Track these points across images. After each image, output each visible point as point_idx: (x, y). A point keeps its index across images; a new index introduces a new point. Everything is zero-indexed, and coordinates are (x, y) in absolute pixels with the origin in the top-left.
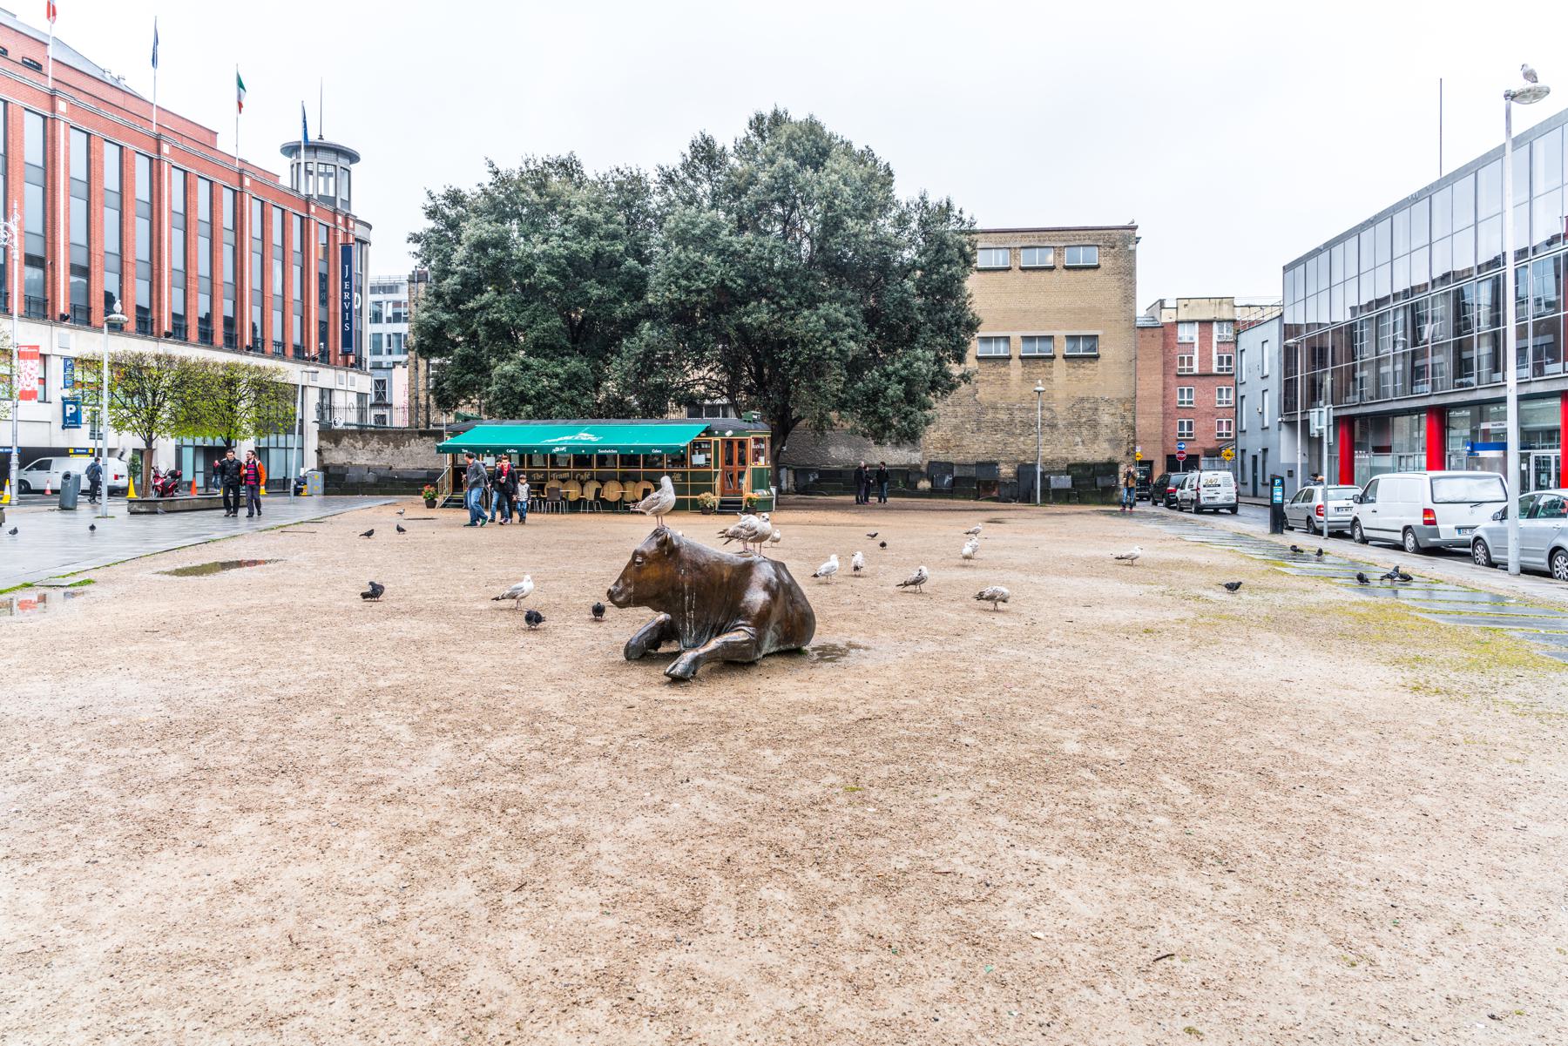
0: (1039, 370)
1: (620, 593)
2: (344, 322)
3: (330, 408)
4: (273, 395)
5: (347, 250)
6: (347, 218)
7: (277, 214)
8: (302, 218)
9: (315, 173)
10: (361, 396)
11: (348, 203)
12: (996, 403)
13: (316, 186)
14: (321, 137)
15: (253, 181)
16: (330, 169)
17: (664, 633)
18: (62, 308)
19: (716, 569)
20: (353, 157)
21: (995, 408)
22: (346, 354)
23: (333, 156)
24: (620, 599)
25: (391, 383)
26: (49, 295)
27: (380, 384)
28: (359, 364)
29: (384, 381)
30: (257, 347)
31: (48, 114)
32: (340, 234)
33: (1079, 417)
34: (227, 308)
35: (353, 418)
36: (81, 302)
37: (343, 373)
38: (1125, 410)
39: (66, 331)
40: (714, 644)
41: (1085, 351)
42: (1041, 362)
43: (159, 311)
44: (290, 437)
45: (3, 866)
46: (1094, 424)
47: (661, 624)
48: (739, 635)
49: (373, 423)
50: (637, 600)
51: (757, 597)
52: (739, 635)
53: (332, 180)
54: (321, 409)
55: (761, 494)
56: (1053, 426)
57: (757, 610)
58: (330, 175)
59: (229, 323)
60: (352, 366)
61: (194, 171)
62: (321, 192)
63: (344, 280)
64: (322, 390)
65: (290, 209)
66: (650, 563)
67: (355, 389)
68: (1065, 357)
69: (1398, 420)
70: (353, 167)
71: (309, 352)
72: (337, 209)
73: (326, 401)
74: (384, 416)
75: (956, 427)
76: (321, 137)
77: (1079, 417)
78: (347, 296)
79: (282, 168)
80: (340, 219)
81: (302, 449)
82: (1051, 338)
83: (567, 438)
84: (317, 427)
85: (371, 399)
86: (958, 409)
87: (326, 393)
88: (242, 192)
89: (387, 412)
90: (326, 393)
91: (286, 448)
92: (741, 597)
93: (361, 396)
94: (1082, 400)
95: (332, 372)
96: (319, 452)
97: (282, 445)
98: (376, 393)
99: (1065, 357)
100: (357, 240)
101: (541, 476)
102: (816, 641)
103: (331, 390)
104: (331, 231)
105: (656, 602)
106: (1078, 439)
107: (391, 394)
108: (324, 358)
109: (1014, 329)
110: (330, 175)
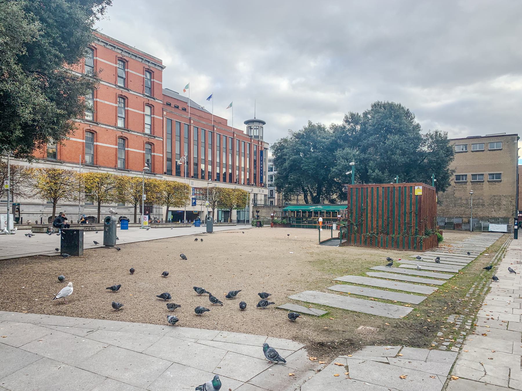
0: (478, 186)
2: (261, 173)
4: (243, 198)
5: (262, 152)
6: (262, 142)
7: (243, 143)
8: (249, 144)
9: (253, 129)
10: (265, 195)
11: (262, 137)
12: (462, 197)
13: (254, 133)
14: (255, 118)
15: (236, 134)
16: (257, 127)
18: (192, 175)
20: (264, 123)
21: (461, 199)
22: (261, 183)
23: (258, 123)
26: (189, 172)
28: (264, 186)
30: (238, 182)
31: (189, 124)
32: (260, 147)
33: (493, 202)
34: (230, 171)
35: (263, 203)
37: (260, 189)
38: (512, 199)
39: (193, 181)
41: (496, 178)
42: (479, 183)
43: (214, 174)
46: (499, 204)
53: (258, 130)
56: (483, 205)
58: (257, 129)
59: (231, 175)
60: (263, 186)
61: (222, 134)
62: (255, 134)
63: (261, 161)
65: (246, 142)
68: (488, 181)
69: (337, 237)
70: (264, 126)
71: (251, 183)
72: (259, 139)
76: (255, 118)
77: (493, 202)
78: (261, 166)
79: (244, 128)
80: (260, 143)
82: (483, 175)
86: (447, 199)
87: (255, 195)
88: (234, 138)
90: (255, 195)
93: (265, 195)
94: (494, 196)
99: (488, 181)
100: (264, 148)
103: (257, 194)
104: (257, 146)
106: (493, 210)
108: (256, 184)
109: (469, 172)
110: (257, 129)
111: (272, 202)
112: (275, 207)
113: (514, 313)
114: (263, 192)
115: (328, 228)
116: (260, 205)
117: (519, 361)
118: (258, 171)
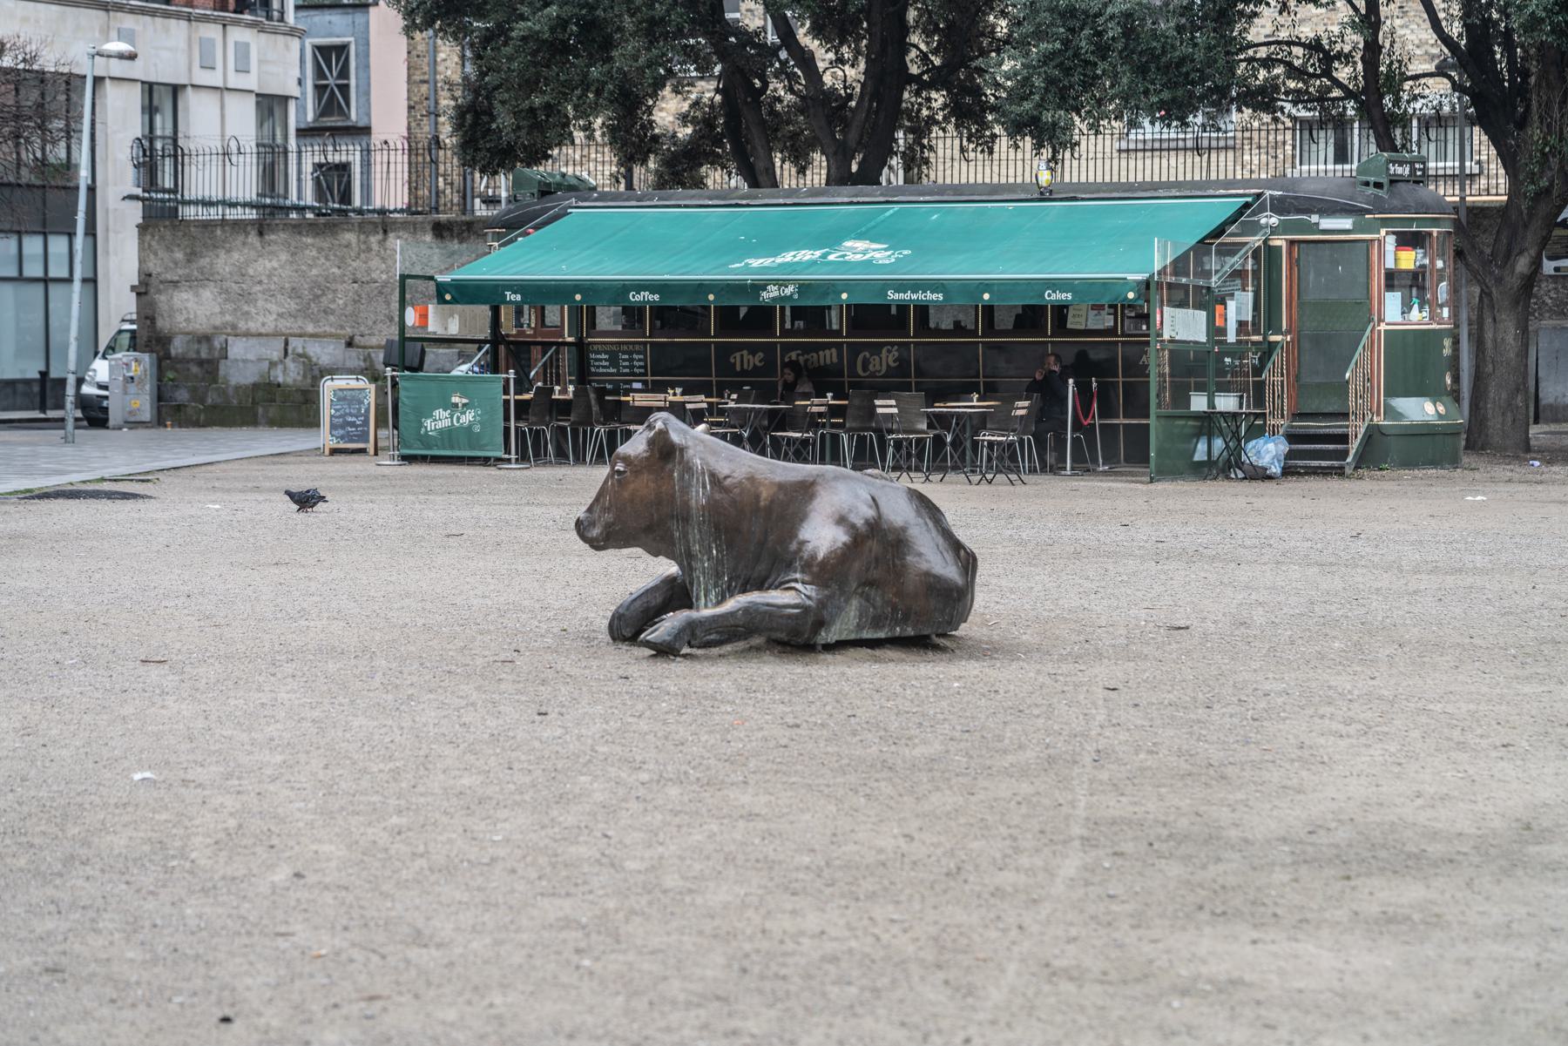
1: (593, 524)
3: (177, 154)
10: (270, 105)
17: (675, 595)
24: (595, 532)
25: (365, 55)
27: (331, 57)
29: (342, 49)
35: (244, 183)
36: (90, 275)
37: (212, 32)
44: (58, 245)
49: (309, 199)
54: (148, 165)
55: (1422, 410)
64: (149, 88)
67: (251, 82)
73: (162, 125)
74: (344, 168)
81: (91, 281)
83: (755, 263)
84: (135, 212)
85: (305, 110)
89: (348, 153)
91: (46, 281)
92: (792, 533)
93: (270, 105)
95: (178, 28)
96: (143, 290)
97: (33, 269)
98: (320, 89)
101: (757, 360)
103: (176, 90)
105: (653, 535)
107: (366, 93)
111: (334, 179)
112: (383, 222)
113: (407, 343)
114: (243, 70)
115: (1110, 458)
116: (214, 214)
117: (841, 633)
118: (1023, 462)
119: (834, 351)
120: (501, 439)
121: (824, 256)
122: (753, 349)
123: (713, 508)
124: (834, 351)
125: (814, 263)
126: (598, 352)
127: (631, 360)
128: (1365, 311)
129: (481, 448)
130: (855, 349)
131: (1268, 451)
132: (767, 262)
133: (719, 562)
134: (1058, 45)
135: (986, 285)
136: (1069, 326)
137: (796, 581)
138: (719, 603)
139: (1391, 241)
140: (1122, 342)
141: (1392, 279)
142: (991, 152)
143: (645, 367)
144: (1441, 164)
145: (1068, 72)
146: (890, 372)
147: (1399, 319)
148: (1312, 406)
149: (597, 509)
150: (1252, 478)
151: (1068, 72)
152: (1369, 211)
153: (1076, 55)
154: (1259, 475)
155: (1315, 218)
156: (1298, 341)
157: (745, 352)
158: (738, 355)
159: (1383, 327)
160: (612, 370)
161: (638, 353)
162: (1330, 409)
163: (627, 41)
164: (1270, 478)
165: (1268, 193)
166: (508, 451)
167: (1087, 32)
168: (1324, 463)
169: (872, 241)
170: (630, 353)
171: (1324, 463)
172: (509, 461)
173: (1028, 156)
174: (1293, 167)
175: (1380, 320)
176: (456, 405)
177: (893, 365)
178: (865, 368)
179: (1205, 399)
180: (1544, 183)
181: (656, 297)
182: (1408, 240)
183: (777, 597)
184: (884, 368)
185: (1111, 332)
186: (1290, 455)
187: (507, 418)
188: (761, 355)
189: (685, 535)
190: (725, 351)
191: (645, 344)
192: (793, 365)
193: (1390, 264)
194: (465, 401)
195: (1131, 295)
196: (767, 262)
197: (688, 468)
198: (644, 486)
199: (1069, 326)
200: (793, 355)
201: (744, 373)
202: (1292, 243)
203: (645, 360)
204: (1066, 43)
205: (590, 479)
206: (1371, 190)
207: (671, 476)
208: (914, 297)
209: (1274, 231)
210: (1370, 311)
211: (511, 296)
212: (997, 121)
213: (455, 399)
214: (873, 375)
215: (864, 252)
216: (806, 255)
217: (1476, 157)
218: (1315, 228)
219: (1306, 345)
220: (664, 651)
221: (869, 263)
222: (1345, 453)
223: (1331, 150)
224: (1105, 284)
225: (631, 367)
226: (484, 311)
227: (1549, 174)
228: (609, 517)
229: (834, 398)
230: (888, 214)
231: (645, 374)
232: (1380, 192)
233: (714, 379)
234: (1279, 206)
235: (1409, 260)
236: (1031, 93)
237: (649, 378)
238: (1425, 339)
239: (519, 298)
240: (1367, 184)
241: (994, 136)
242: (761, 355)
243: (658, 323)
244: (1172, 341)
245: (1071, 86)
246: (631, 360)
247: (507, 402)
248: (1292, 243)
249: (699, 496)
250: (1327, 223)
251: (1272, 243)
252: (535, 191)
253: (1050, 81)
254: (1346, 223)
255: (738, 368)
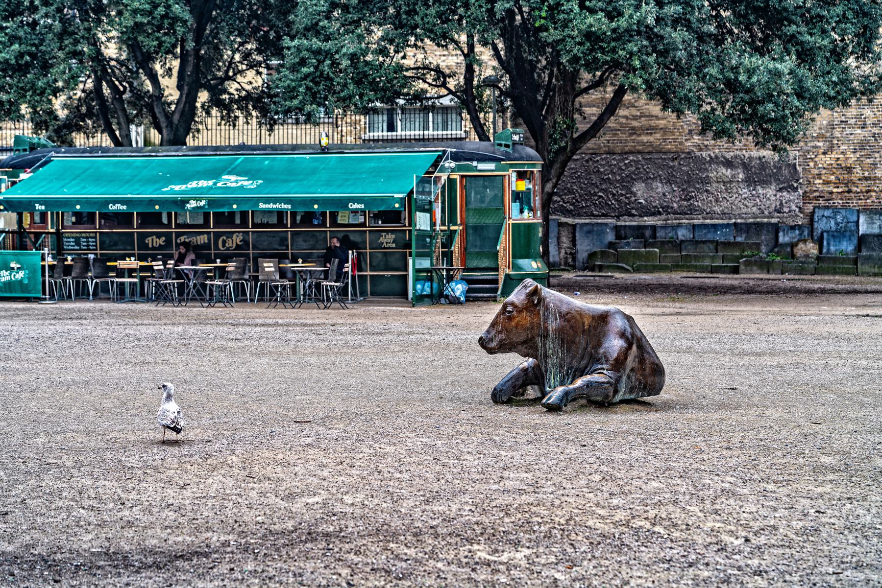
1: (491, 340)
19: (578, 317)
24: (493, 344)
40: (579, 382)
45: (879, 173)
47: (525, 370)
48: (600, 377)
50: (504, 347)
51: (614, 345)
52: (600, 377)
57: (615, 355)
66: (520, 311)
75: (862, 145)
83: (177, 188)
92: (599, 344)
101: (161, 241)
102: (664, 395)
105: (527, 347)
119: (206, 236)
120: (41, 287)
121: (215, 184)
122: (159, 235)
123: (560, 331)
124: (206, 236)
125: (211, 188)
126: (69, 238)
127: (88, 242)
128: (500, 210)
129: (29, 292)
130: (218, 235)
131: (458, 289)
132: (183, 187)
133: (562, 359)
134: (312, 69)
135: (316, 201)
136: (339, 222)
137: (603, 369)
138: (572, 383)
139: (514, 177)
140: (370, 231)
141: (517, 196)
142: (234, 126)
143: (96, 246)
144: (445, 132)
145: (317, 84)
146: (238, 247)
147: (519, 217)
148: (474, 263)
149: (493, 333)
150: (451, 303)
151: (317, 84)
152: (503, 160)
153: (322, 73)
154: (454, 301)
155: (475, 163)
156: (466, 228)
157: (154, 237)
158: (150, 239)
159: (511, 221)
160: (76, 247)
161: (92, 238)
162: (483, 266)
163: (60, 64)
164: (460, 303)
165: (449, 150)
166: (44, 293)
167: (328, 62)
168: (485, 295)
169: (238, 175)
170: (87, 238)
171: (485, 295)
172: (45, 299)
173: (254, 127)
174: (365, 133)
175: (509, 218)
176: (13, 268)
177: (239, 243)
178: (224, 246)
179: (429, 262)
180: (563, 144)
181: (125, 207)
182: (521, 176)
183: (595, 377)
184: (234, 245)
185: (363, 225)
186: (469, 291)
187: (43, 275)
188: (164, 238)
189: (544, 345)
190: (142, 236)
191: (96, 233)
192: (185, 244)
193: (514, 188)
194: (19, 266)
195: (397, 205)
196: (183, 187)
197: (547, 308)
198: (525, 319)
199: (339, 222)
200: (182, 238)
201: (154, 248)
202: (462, 177)
203: (96, 242)
204: (316, 68)
205: (489, 313)
206: (503, 149)
207: (539, 313)
208: (275, 206)
209: (453, 170)
210: (505, 213)
211: (39, 207)
212: (238, 109)
213: (12, 265)
214: (228, 249)
215: (236, 181)
216: (203, 183)
217: (463, 129)
218: (475, 169)
219: (471, 231)
220: (553, 409)
221: (242, 187)
222: (497, 289)
223: (385, 125)
224: (383, 200)
225: (88, 246)
226: (14, 216)
227: (565, 139)
228: (502, 336)
229: (221, 262)
230: (239, 161)
231: (96, 250)
232: (508, 150)
233: (251, 252)
234: (455, 157)
235: (522, 186)
236: (298, 95)
237: (98, 252)
238: (529, 227)
239: (43, 207)
240: (500, 145)
241: (237, 117)
242: (164, 238)
243: (103, 221)
244: (419, 230)
245: (319, 92)
246: (88, 242)
247: (43, 267)
248: (462, 177)
249: (553, 325)
250: (482, 166)
251: (451, 177)
252: (27, 148)
253: (308, 88)
254: (491, 166)
255: (150, 246)
